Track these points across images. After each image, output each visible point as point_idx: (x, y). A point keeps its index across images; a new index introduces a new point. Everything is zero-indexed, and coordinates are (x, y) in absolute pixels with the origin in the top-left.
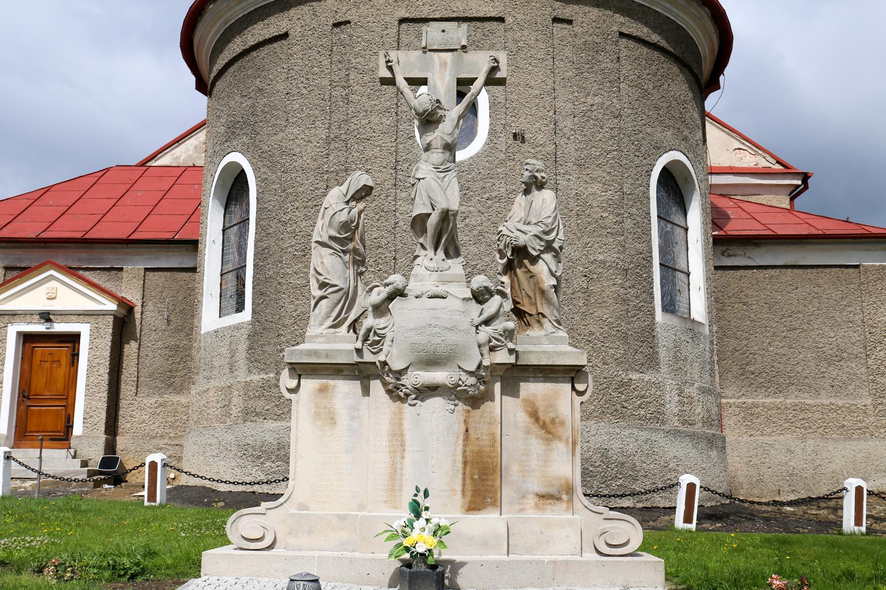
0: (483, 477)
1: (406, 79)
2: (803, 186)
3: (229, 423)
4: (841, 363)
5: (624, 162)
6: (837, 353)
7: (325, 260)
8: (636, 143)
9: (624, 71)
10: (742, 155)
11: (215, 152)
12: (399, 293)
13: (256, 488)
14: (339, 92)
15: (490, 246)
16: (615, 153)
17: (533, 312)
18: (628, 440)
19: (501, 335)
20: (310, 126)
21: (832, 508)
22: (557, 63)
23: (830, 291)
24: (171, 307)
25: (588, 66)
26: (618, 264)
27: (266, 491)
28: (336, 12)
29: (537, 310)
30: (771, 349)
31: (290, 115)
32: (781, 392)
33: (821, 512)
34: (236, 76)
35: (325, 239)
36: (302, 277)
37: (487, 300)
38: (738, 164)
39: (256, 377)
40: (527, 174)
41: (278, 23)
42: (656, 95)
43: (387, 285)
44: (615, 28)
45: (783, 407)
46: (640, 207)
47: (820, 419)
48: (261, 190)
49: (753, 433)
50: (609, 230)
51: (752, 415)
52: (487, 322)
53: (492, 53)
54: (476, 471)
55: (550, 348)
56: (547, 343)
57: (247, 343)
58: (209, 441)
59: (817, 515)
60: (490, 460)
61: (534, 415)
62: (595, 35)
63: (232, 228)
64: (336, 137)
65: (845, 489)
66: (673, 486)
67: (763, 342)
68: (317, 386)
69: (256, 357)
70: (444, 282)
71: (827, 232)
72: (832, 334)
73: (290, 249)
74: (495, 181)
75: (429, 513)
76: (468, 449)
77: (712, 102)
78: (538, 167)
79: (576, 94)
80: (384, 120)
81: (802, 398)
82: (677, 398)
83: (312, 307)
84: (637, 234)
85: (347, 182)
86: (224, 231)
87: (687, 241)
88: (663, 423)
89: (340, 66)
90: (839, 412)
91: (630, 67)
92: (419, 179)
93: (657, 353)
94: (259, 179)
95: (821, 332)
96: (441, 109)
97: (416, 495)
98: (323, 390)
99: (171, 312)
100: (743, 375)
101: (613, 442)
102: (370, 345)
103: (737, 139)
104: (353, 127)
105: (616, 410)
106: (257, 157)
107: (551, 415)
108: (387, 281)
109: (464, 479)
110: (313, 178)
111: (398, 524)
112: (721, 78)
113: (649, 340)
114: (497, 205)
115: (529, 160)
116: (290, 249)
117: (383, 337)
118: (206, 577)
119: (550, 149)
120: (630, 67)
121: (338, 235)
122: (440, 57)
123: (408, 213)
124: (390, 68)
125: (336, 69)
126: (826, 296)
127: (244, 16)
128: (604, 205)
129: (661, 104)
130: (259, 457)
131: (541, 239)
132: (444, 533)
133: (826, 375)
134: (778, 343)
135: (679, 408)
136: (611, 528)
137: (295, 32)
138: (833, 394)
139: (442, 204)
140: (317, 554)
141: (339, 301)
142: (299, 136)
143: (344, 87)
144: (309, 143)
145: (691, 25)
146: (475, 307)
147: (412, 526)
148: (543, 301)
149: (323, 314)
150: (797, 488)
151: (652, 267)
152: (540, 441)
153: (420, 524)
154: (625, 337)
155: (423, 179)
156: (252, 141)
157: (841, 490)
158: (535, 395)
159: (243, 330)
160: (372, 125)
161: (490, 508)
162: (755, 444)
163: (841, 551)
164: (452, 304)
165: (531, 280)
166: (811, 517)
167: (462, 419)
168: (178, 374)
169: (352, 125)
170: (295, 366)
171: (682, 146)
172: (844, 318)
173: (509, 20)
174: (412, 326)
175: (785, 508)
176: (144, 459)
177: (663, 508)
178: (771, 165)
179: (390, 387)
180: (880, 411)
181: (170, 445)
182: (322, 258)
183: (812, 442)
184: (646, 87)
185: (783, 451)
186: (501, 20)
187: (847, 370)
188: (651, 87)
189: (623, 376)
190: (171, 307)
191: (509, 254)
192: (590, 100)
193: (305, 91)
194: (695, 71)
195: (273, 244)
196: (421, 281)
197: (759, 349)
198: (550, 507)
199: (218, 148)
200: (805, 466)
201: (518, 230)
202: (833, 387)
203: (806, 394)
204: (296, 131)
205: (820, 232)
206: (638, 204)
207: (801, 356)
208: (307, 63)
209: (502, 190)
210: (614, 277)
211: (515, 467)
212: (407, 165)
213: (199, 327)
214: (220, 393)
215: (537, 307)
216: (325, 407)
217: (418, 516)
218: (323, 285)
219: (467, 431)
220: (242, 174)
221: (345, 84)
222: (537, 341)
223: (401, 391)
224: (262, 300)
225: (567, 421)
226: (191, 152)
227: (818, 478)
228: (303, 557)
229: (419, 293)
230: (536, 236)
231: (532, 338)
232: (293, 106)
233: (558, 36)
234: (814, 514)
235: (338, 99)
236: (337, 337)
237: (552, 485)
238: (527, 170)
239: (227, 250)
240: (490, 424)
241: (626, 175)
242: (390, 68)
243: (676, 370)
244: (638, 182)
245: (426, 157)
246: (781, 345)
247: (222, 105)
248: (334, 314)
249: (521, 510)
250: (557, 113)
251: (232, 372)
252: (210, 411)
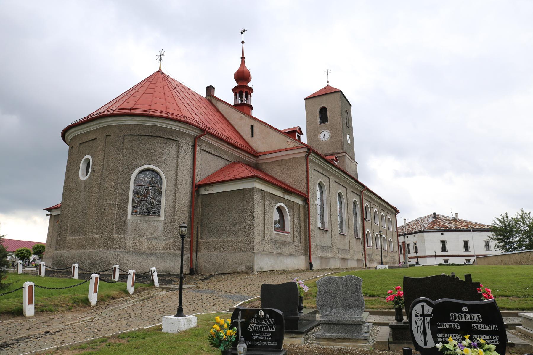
26: (114, 203)
93: (127, 228)
100: (208, 231)
178: (299, 145)
180: (245, 242)
192: (112, 157)
202: (233, 234)
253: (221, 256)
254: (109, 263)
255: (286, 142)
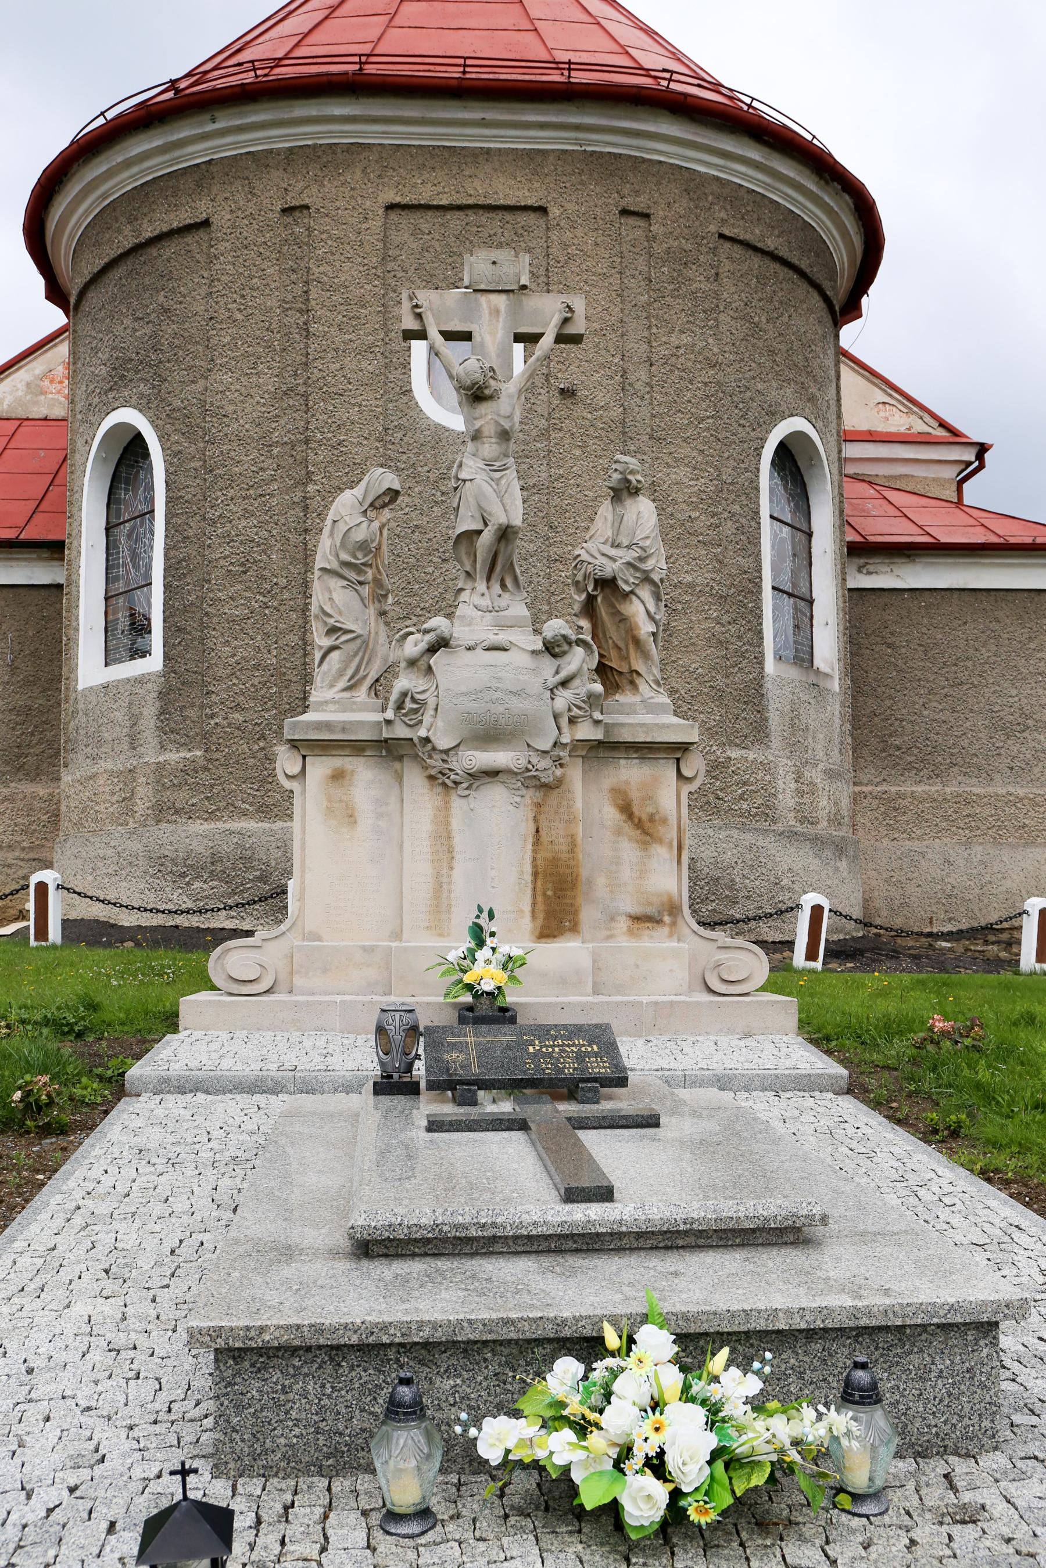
0: (559, 893)
1: (442, 333)
2: (977, 464)
3: (131, 825)
4: (1025, 734)
5: (724, 434)
6: (1020, 720)
7: (335, 596)
8: (741, 405)
9: (725, 295)
10: (887, 414)
11: (90, 405)
12: (441, 644)
13: (180, 920)
14: (294, 318)
15: (526, 559)
16: (711, 421)
17: (625, 669)
18: (724, 845)
19: (583, 701)
20: (248, 371)
21: (1004, 942)
22: (626, 281)
23: (1012, 629)
24: (17, 647)
25: (672, 287)
27: (195, 924)
28: (286, 189)
29: (630, 666)
30: (926, 713)
31: (216, 353)
32: (937, 776)
33: (990, 947)
34: (124, 285)
35: (335, 565)
36: (242, 605)
37: (565, 653)
38: (881, 427)
39: (174, 756)
40: (616, 476)
41: (193, 205)
42: (771, 332)
43: (427, 632)
44: (713, 228)
45: (941, 798)
46: (745, 503)
47: (992, 816)
48: (172, 470)
49: (896, 836)
50: (701, 538)
51: (895, 809)
52: (564, 684)
53: (564, 298)
54: (550, 886)
55: (648, 719)
56: (644, 711)
57: (158, 704)
58: (101, 853)
59: (983, 951)
60: (568, 871)
61: (626, 809)
62: (684, 238)
63: (122, 527)
64: (291, 389)
65: (1026, 912)
66: (792, 909)
67: (914, 703)
68: (329, 772)
69: (173, 725)
70: (502, 626)
71: (1012, 540)
72: (1014, 692)
73: (222, 562)
74: (533, 461)
75: (495, 940)
76: (539, 856)
77: (850, 335)
78: (631, 467)
79: (654, 330)
80: (364, 364)
81: (968, 785)
82: (793, 785)
83: (317, 663)
84: (741, 543)
85: (363, 484)
86: (107, 530)
87: (810, 553)
88: (774, 821)
89: (294, 277)
90: (1019, 805)
91: (733, 289)
92: (464, 481)
93: (766, 719)
94: (169, 452)
95: (997, 688)
96: (495, 379)
97: (478, 917)
98: (338, 776)
99: (16, 654)
100: (884, 751)
101: (702, 849)
102: (405, 715)
103: (880, 388)
104: (317, 374)
105: (708, 803)
106: (164, 416)
107: (650, 809)
108: (426, 626)
109: (534, 896)
110: (255, 453)
111: (453, 956)
112: (864, 300)
113: (755, 701)
114: (536, 498)
115: (619, 457)
116: (222, 562)
117: (423, 704)
118: (188, 1032)
119: (615, 414)
120: (733, 289)
121: (353, 561)
122: (489, 302)
123: (402, 509)
124: (419, 316)
125: (288, 282)
126: (1006, 636)
127: (135, 188)
128: (694, 499)
129: (779, 346)
130: (183, 875)
131: (636, 569)
132: (517, 965)
133: (1002, 751)
134: (935, 704)
135: (797, 799)
136: (727, 959)
137: (222, 219)
138: (1012, 779)
139: (499, 518)
140: (338, 998)
141: (356, 654)
142: (232, 387)
143: (300, 311)
144: (248, 399)
145: (823, 222)
146: (548, 665)
147: (474, 956)
148: (638, 654)
149: (333, 672)
150: (957, 915)
151: (760, 593)
152: (635, 845)
153: (482, 954)
154: (719, 695)
155: (471, 480)
156: (156, 391)
157: (1020, 914)
158: (627, 782)
159: (149, 685)
160: (346, 371)
161: (568, 935)
162: (898, 853)
163: (1018, 994)
164: (518, 659)
165: (622, 625)
166: (977, 955)
167: (531, 815)
168: (32, 751)
169: (315, 371)
170: (296, 743)
171: (807, 410)
172: (1031, 669)
173: (554, 211)
174: (463, 689)
175: (939, 943)
176: (26, 877)
177: (773, 942)
178: (930, 430)
179: (433, 772)
181: (23, 860)
182: (330, 592)
183: (980, 848)
184: (756, 319)
185: (939, 862)
186: (542, 210)
187: (1032, 744)
188: (764, 320)
189: (718, 753)
190: (17, 647)
191: (590, 589)
192: (674, 339)
193: (239, 316)
194: (828, 293)
195: (195, 553)
196: (470, 625)
197: (909, 713)
198: (647, 932)
199: (97, 399)
200: (969, 883)
201: (603, 555)
202: (1012, 769)
203: (974, 779)
204: (227, 378)
205: (1002, 541)
206: (743, 498)
207: (968, 724)
208: (240, 270)
209: (544, 475)
210: (707, 607)
211: (601, 881)
212: (399, 435)
213: (72, 678)
214: (116, 780)
215: (629, 663)
216: (341, 801)
217: (481, 944)
218: (333, 630)
219: (537, 831)
220: (138, 439)
221: (303, 307)
222: (631, 710)
223: (448, 778)
224: (179, 640)
225: (670, 818)
226: (20, 393)
227: (986, 901)
228: (320, 1003)
229: (472, 643)
230: (629, 564)
231: (622, 705)
232: (222, 339)
233: (628, 238)
234: (978, 951)
235: (292, 330)
236: (354, 703)
237: (650, 904)
238: (616, 470)
239: (114, 560)
240: (569, 821)
241: (726, 455)
242: (419, 316)
243: (795, 746)
244: (742, 466)
245: (474, 449)
246: (940, 707)
247: (101, 331)
248: (350, 672)
249: (609, 937)
250: (626, 359)
251: (134, 748)
252: (101, 808)
253: (967, 860)
254: (731, 888)
255: (872, 405)
